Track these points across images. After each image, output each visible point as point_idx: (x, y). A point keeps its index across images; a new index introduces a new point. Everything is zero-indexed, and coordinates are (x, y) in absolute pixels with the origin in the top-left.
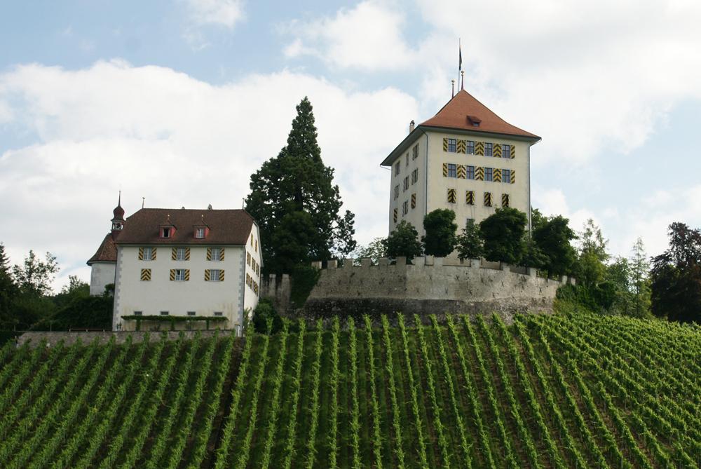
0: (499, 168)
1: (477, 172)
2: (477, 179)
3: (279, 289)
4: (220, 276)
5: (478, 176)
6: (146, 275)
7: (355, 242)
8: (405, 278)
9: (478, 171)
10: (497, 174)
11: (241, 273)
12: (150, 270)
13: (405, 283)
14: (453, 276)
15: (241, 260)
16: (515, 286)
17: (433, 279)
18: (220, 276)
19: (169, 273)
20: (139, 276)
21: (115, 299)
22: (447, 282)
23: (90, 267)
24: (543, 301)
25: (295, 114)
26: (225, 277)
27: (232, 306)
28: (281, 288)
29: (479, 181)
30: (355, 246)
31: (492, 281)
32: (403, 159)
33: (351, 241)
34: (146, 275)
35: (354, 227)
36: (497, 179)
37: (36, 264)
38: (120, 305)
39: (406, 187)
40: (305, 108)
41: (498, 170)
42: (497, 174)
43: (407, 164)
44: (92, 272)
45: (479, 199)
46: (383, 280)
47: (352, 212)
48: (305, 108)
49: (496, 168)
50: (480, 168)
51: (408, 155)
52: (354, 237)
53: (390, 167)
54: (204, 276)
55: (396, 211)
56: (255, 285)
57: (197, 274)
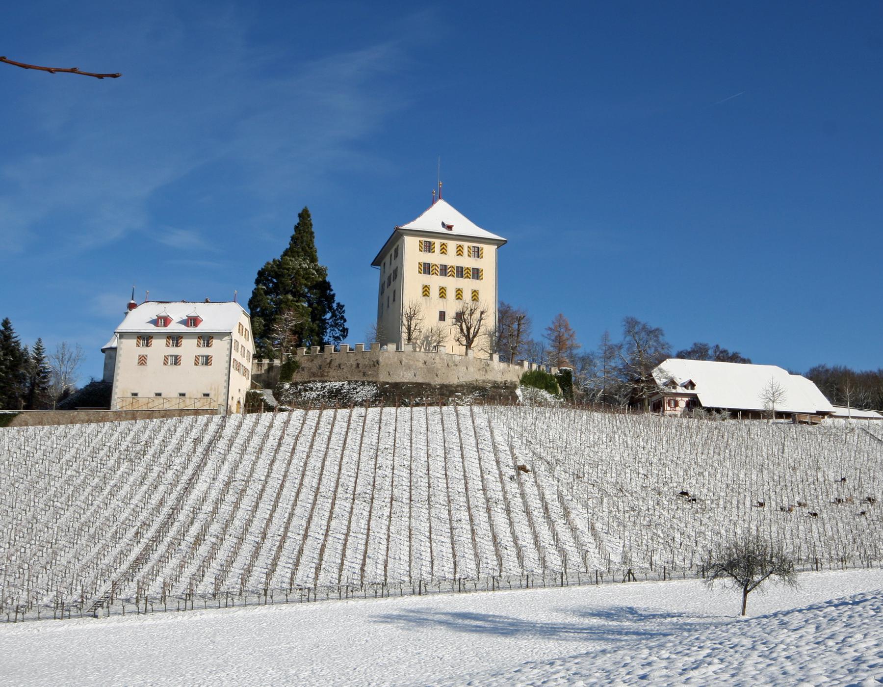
0: (469, 267)
1: (449, 270)
2: (449, 276)
3: (271, 373)
4: (207, 361)
5: (450, 273)
6: (143, 360)
7: (347, 330)
8: (378, 363)
9: (450, 269)
10: (468, 272)
11: (227, 359)
12: (146, 356)
13: (378, 368)
14: (422, 361)
15: (228, 346)
16: (479, 370)
17: (403, 363)
18: (207, 361)
19: (148, 362)
20: (137, 361)
21: (114, 382)
22: (416, 367)
23: (104, 354)
24: (505, 384)
25: (297, 221)
26: (212, 362)
27: (218, 389)
28: (272, 372)
29: (451, 278)
30: (347, 333)
31: (456, 365)
32: (387, 259)
33: (344, 328)
34: (143, 360)
35: (346, 315)
36: (468, 277)
37: (240, 537)
38: (119, 387)
39: (389, 284)
40: (304, 216)
41: (468, 268)
42: (468, 272)
43: (391, 264)
44: (106, 359)
45: (451, 294)
46: (358, 365)
47: (342, 303)
48: (304, 216)
49: (467, 266)
50: (452, 267)
51: (391, 255)
52: (346, 325)
53: (379, 267)
54: (148, 359)
55: (394, 300)
56: (245, 370)
57: (187, 359)
